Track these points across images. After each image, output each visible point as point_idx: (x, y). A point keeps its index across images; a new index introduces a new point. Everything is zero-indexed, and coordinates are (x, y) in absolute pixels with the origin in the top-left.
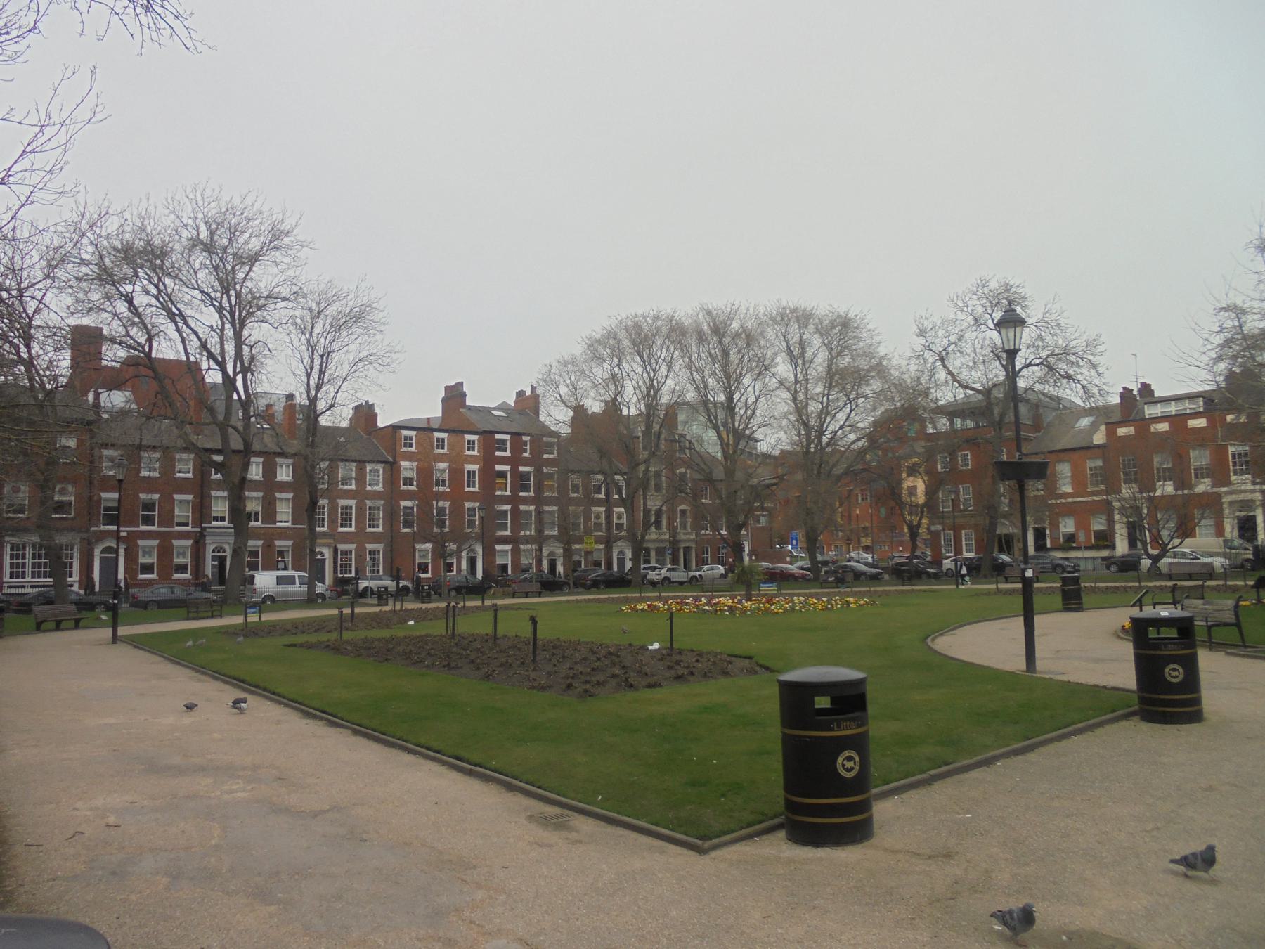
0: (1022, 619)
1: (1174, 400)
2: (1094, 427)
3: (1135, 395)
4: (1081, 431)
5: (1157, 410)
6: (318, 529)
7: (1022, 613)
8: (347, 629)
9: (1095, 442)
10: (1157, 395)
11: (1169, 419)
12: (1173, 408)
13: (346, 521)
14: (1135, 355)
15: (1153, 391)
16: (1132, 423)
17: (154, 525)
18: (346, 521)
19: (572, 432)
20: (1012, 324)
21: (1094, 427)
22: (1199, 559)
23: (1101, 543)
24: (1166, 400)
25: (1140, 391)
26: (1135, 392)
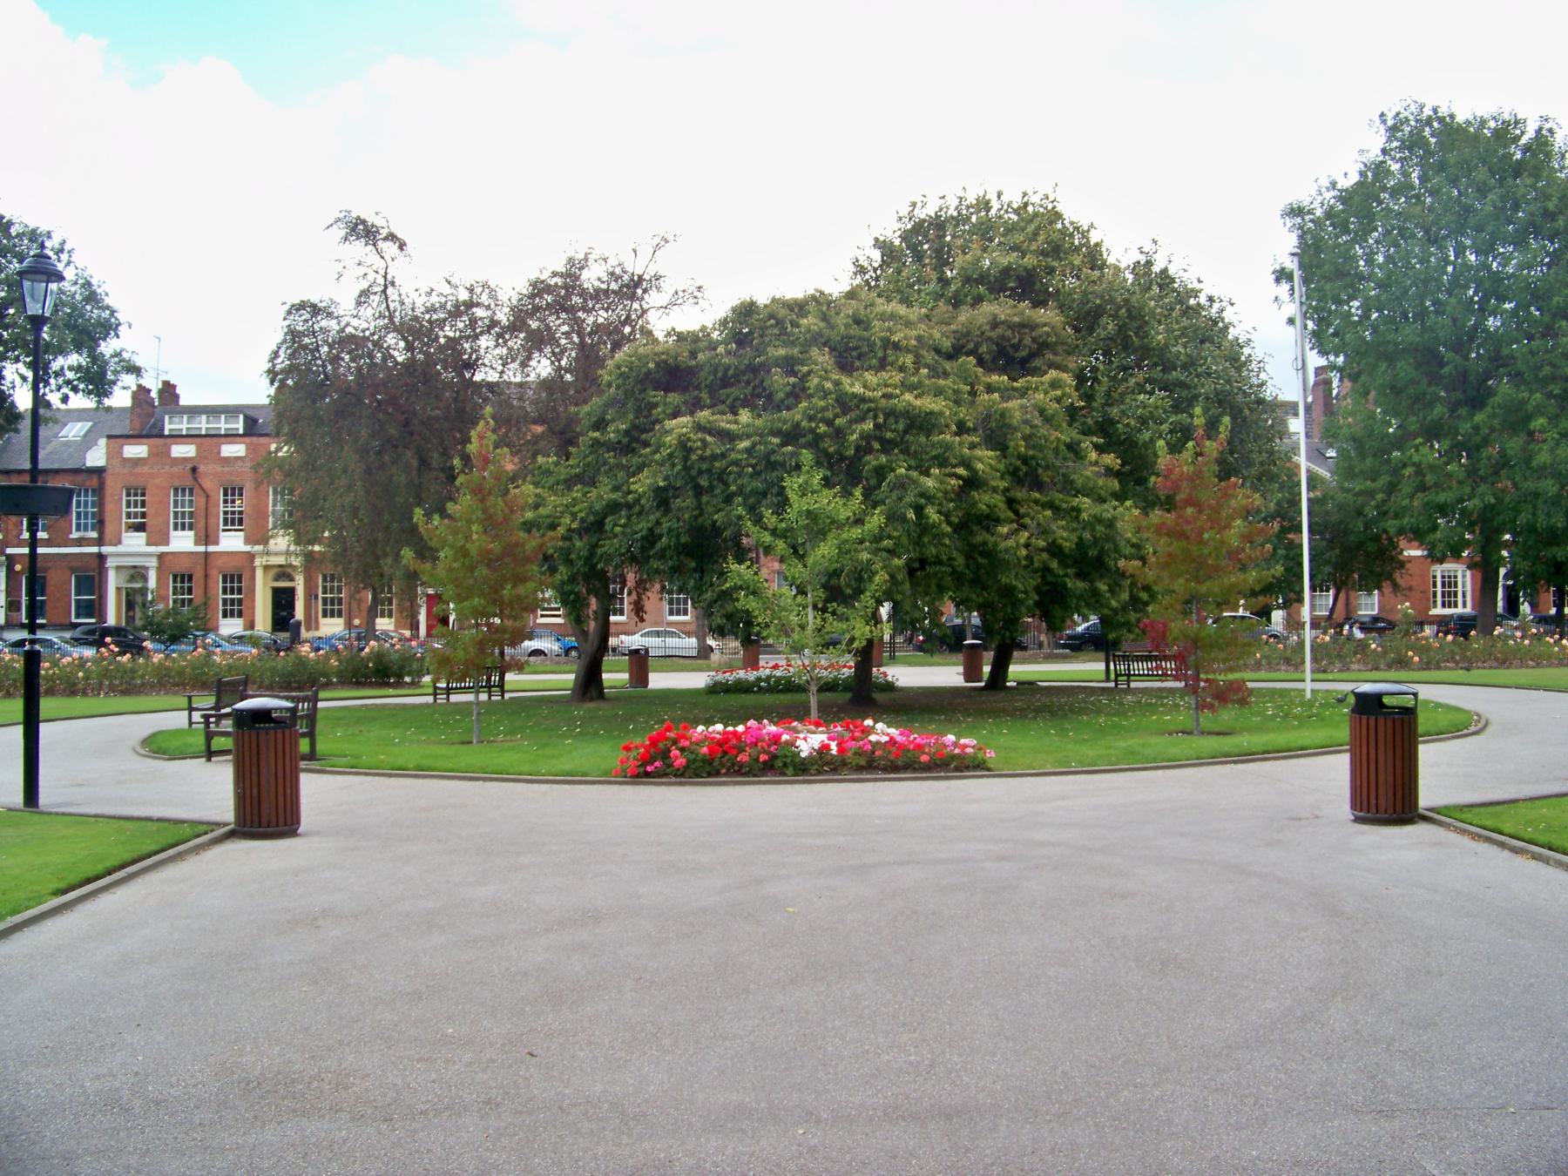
0: (20, 729)
1: (205, 413)
2: (88, 441)
3: (153, 399)
4: (68, 444)
5: (183, 425)
6: (612, 618)
7: (21, 720)
8: (72, 689)
9: (89, 464)
10: (183, 402)
11: (198, 440)
12: (203, 424)
13: (332, 603)
14: (159, 338)
15: (177, 397)
16: (145, 440)
17: (76, 595)
18: (332, 603)
19: (408, 545)
20: (44, 278)
21: (88, 441)
22: (642, 636)
23: (97, 611)
24: (194, 411)
25: (161, 392)
26: (154, 394)
